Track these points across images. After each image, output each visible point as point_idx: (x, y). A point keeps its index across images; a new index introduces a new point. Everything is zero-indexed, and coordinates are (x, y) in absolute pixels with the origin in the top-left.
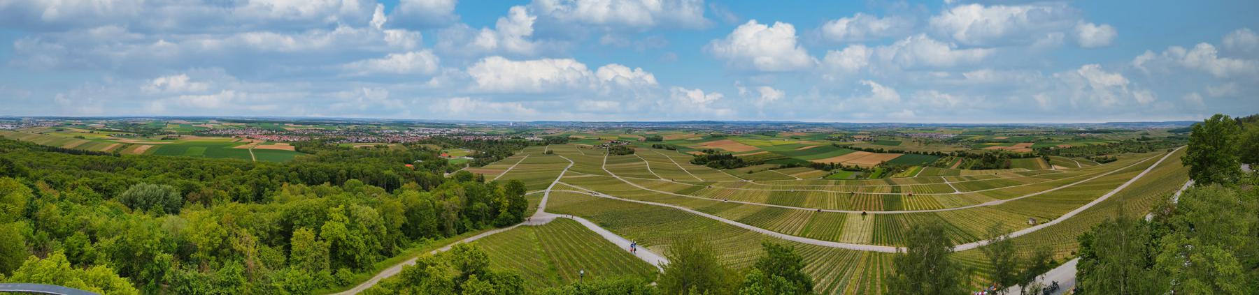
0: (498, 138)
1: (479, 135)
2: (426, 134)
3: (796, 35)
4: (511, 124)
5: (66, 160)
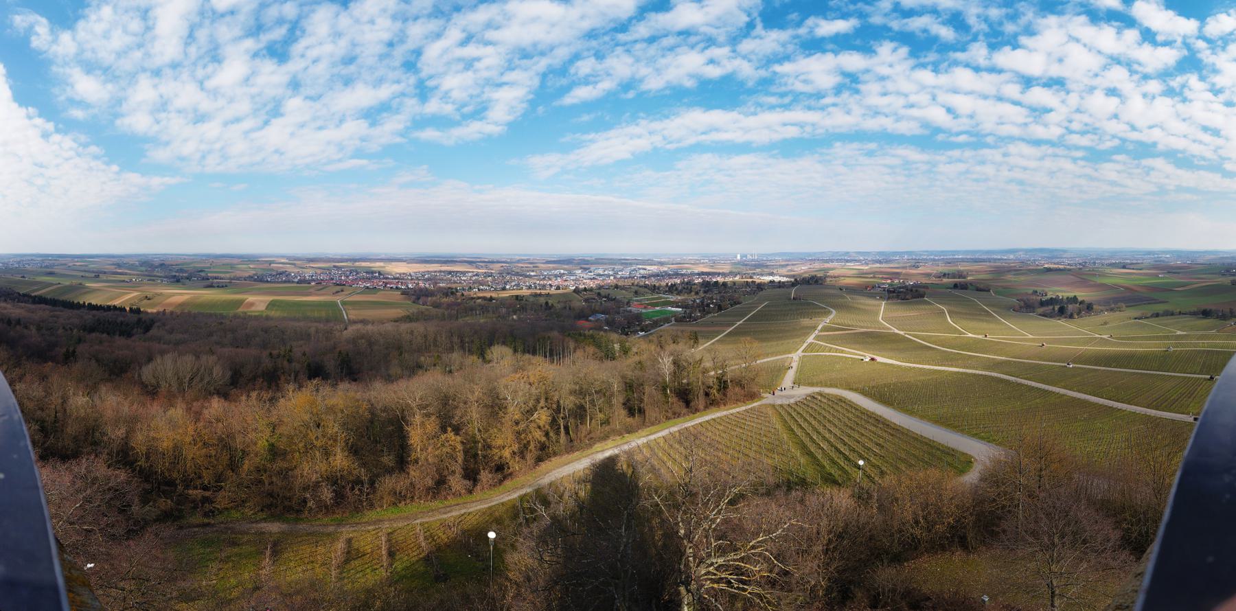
0: (720, 279)
1: (688, 275)
2: (609, 276)
3: (963, 20)
4: (739, 257)
5: (58, 318)
